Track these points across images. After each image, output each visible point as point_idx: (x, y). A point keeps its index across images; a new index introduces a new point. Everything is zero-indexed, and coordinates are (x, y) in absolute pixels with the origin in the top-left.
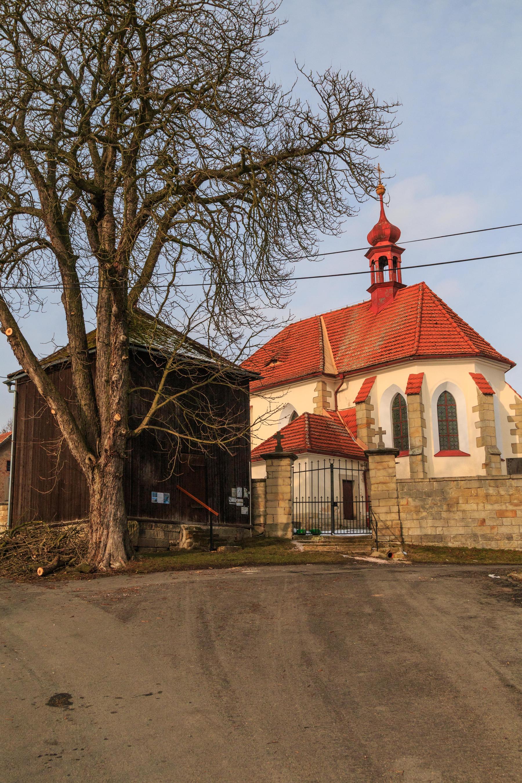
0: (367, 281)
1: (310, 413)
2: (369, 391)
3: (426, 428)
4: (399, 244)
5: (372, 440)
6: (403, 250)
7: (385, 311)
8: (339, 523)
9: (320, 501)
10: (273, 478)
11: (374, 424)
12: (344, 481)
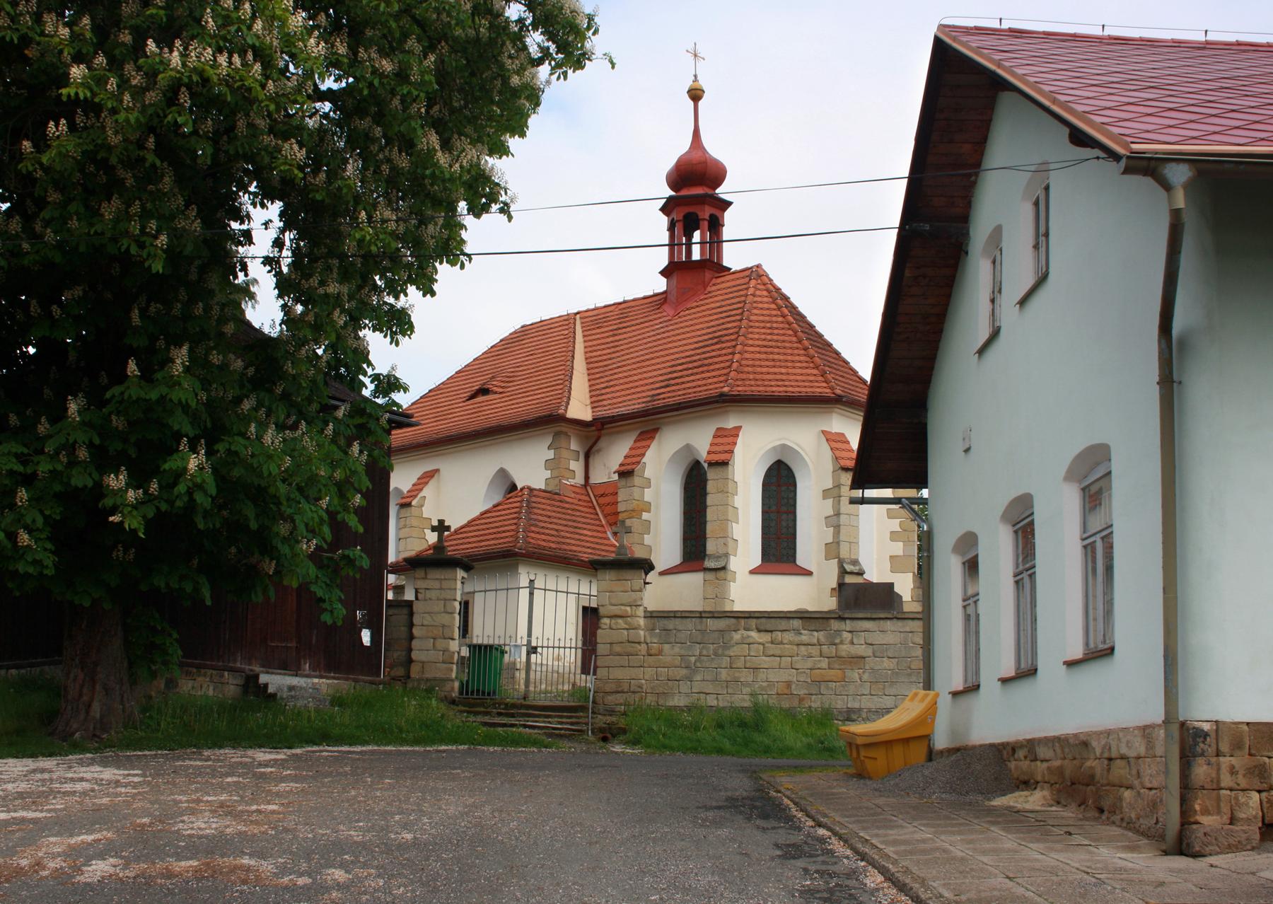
0: (662, 258)
1: (534, 486)
2: (643, 455)
3: (737, 523)
4: (723, 191)
5: (643, 539)
6: (729, 204)
7: (687, 312)
8: (572, 680)
9: (556, 645)
10: (425, 600)
11: (649, 511)
12: (585, 609)
